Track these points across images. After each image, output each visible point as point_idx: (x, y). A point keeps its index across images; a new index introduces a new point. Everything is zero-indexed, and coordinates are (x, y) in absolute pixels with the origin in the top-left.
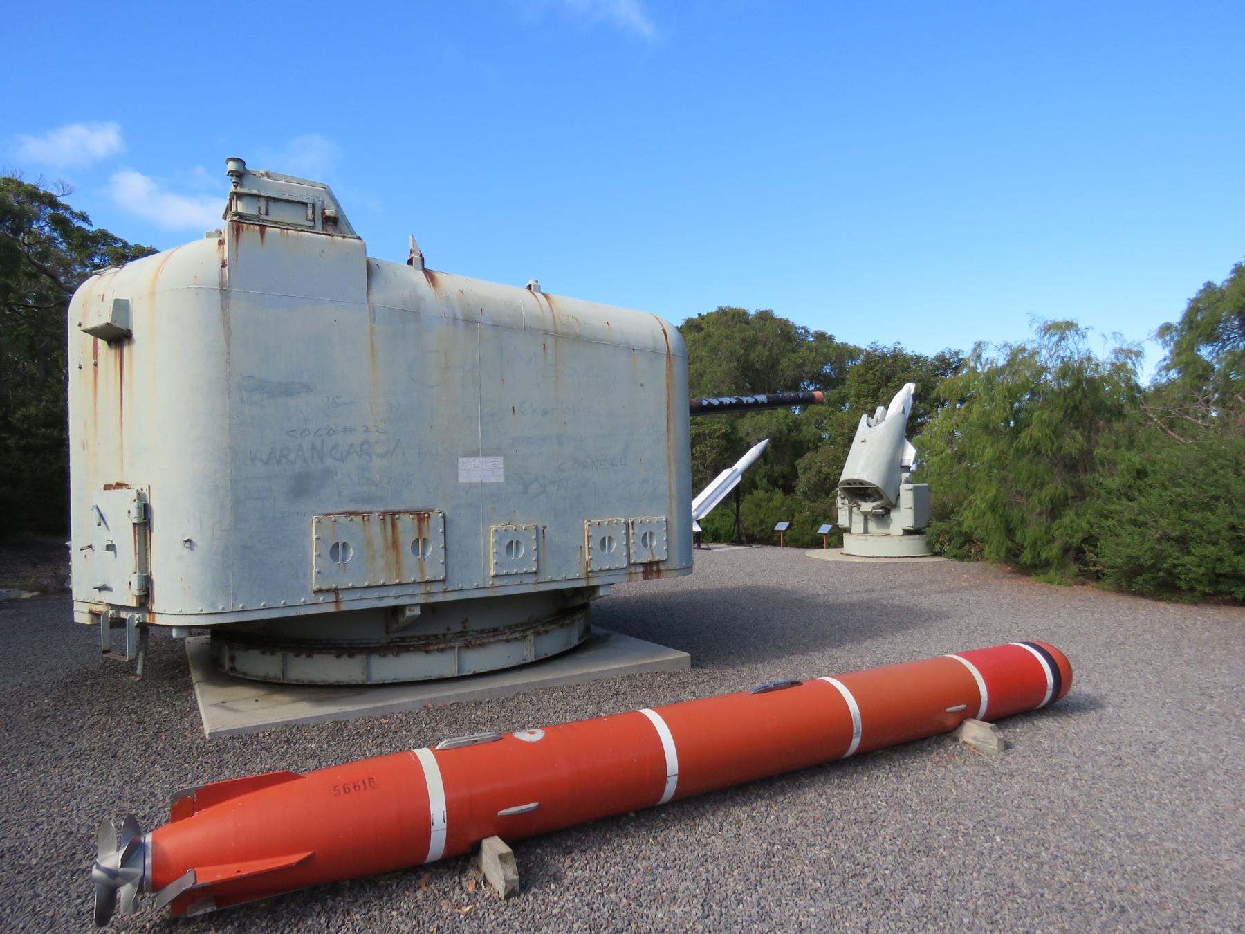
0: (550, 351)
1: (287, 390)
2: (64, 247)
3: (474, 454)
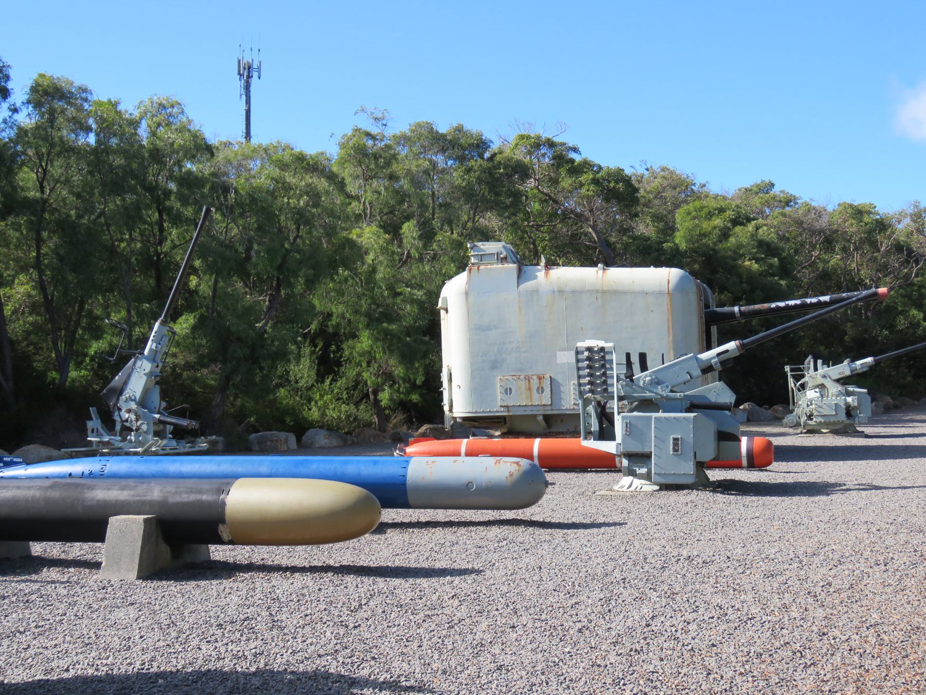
0: (600, 300)
1: (488, 328)
2: (756, 266)
3: (564, 350)
